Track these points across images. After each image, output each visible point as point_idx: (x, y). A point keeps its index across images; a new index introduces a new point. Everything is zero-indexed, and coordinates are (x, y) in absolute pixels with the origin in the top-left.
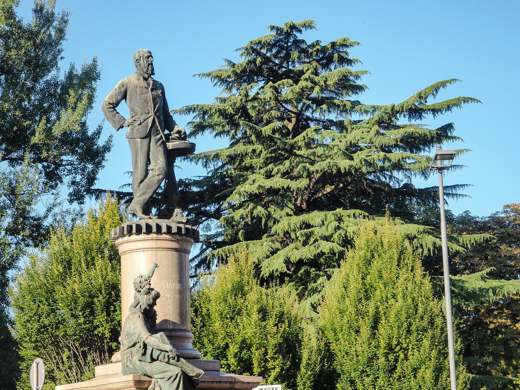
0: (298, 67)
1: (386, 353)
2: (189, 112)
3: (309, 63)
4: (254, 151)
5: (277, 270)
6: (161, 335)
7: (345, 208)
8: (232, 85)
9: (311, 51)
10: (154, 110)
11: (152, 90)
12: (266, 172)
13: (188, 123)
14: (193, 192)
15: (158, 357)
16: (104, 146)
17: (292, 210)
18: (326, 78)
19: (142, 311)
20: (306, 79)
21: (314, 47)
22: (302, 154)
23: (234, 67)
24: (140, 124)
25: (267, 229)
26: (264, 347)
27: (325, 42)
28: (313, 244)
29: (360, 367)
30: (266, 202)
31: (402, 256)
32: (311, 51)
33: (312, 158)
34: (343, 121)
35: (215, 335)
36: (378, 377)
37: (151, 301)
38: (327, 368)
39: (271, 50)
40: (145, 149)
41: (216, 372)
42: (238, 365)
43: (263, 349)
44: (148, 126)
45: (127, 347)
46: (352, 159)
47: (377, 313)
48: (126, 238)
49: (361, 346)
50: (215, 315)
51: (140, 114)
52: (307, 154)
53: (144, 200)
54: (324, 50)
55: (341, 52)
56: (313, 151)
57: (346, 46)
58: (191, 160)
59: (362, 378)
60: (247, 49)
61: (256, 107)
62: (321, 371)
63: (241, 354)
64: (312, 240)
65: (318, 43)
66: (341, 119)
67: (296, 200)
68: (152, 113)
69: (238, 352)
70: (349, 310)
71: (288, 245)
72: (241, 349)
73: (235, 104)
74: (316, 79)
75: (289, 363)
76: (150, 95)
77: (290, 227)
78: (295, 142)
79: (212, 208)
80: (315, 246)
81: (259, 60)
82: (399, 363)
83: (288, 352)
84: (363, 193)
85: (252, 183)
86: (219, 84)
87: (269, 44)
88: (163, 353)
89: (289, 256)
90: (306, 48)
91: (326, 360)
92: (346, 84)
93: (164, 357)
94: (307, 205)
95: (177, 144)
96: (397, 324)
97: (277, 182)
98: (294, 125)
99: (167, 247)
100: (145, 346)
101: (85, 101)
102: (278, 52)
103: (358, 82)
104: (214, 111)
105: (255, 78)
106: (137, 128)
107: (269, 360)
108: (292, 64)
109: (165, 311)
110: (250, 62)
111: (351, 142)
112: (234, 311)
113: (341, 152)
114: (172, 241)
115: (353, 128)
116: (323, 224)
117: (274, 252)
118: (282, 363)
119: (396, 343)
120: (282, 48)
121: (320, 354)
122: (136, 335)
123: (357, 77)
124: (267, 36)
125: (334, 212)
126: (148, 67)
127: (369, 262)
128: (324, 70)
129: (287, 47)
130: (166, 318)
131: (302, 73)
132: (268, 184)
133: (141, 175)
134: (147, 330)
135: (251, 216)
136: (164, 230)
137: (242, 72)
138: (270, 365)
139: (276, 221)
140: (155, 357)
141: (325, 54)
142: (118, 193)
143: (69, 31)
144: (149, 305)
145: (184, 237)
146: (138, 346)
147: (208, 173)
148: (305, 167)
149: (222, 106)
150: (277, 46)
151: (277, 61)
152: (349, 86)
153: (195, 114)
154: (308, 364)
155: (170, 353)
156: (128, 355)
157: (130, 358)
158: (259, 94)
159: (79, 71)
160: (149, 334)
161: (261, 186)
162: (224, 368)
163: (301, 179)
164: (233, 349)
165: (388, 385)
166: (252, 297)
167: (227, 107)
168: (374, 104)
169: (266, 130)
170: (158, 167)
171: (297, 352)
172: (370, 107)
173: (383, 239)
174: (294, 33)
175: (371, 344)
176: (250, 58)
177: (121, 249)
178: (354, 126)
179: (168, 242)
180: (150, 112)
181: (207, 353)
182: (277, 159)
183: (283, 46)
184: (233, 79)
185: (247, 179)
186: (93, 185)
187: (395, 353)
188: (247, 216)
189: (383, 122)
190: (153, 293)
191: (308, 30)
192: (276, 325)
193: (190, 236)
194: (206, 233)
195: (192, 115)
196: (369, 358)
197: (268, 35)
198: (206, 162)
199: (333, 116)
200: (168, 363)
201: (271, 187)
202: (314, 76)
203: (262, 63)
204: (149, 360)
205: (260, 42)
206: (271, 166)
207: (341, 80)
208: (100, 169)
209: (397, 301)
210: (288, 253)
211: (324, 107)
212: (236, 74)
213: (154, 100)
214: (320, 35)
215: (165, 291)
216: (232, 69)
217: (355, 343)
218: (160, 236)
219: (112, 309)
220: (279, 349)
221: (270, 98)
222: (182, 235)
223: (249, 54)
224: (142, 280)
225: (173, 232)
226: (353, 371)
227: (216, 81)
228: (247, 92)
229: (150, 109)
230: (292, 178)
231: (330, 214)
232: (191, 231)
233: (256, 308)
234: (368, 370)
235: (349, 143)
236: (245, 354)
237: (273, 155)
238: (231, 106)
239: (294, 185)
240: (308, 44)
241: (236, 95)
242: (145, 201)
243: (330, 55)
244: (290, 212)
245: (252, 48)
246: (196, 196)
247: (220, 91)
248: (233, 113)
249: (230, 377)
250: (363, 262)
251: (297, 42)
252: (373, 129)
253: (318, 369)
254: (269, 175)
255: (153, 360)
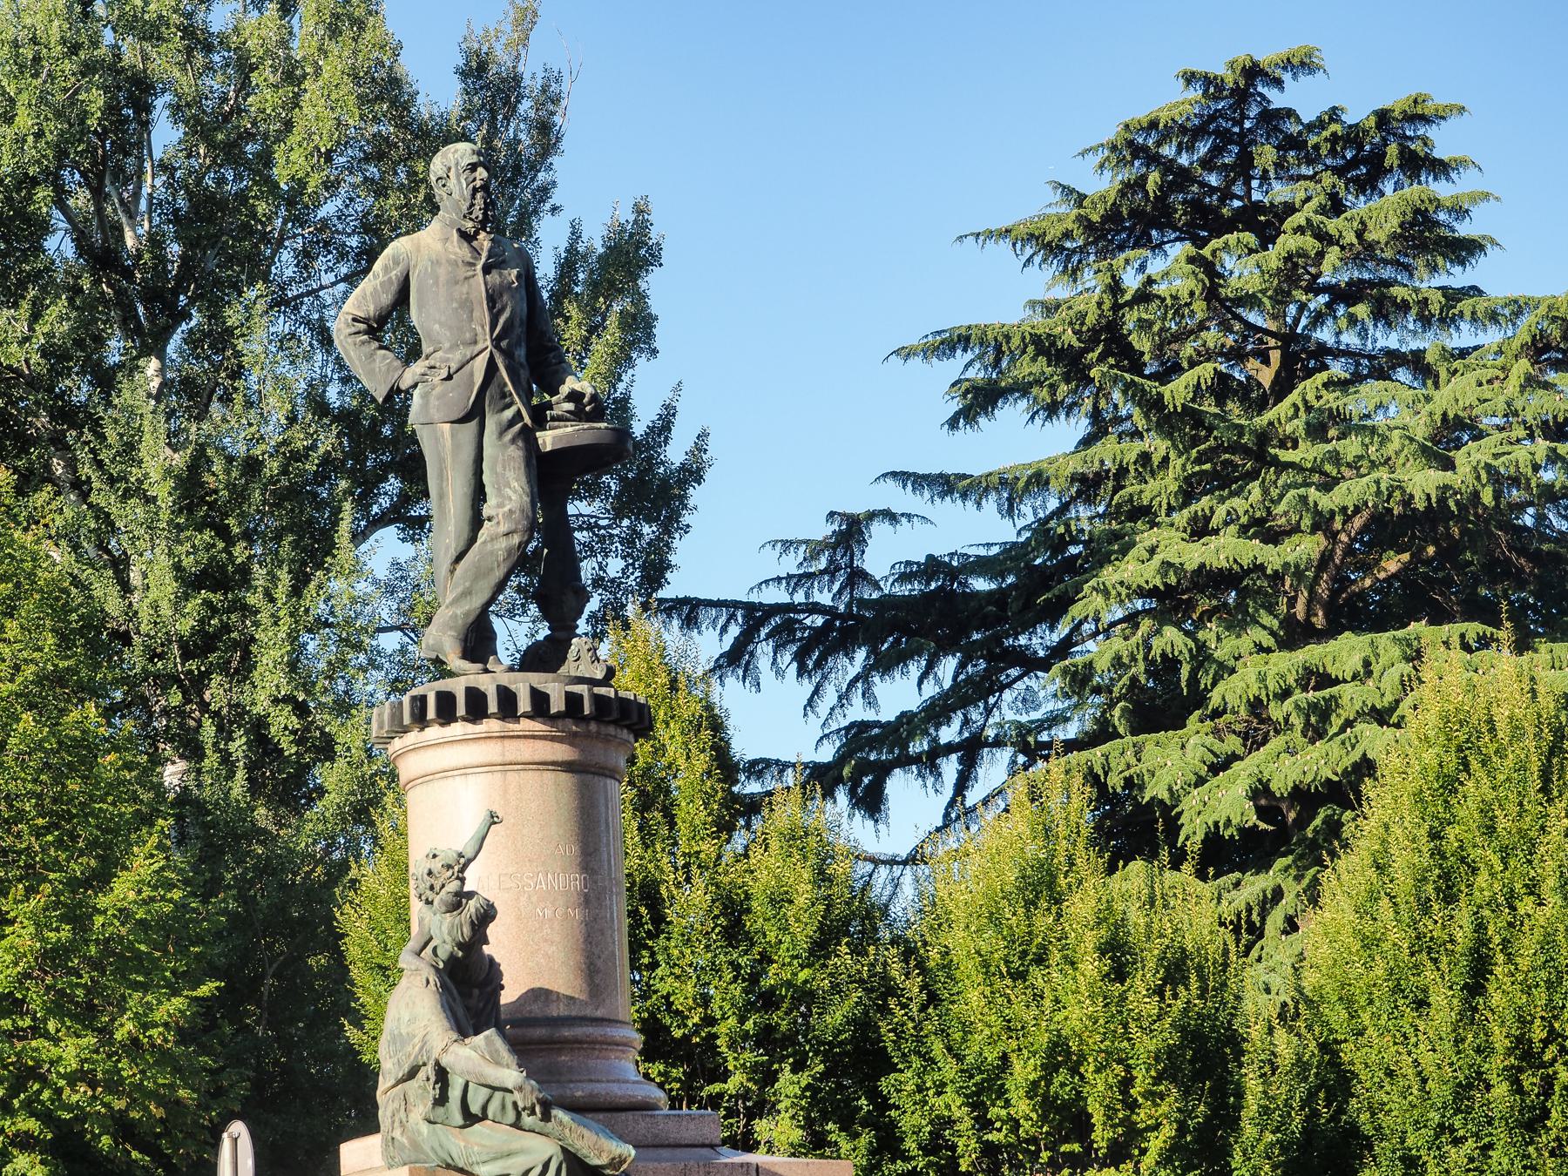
0: (1281, 192)
1: (1513, 1067)
2: (953, 349)
3: (1311, 178)
4: (1145, 458)
5: (1229, 821)
6: (487, 1038)
7: (1435, 620)
8: (1080, 261)
9: (1313, 140)
10: (492, 329)
11: (487, 270)
12: (1194, 519)
13: (953, 385)
14: (976, 595)
15: (484, 1108)
16: (683, 467)
17: (1273, 633)
18: (1362, 223)
19: (441, 965)
20: (1299, 230)
21: (1323, 129)
22: (1297, 460)
23: (1080, 206)
24: (449, 377)
25: (1198, 698)
26: (1120, 1061)
27: (1357, 113)
28: (1337, 734)
29: (1432, 1115)
30: (1203, 613)
31: (1555, 761)
32: (1313, 140)
33: (1328, 468)
34: (1425, 350)
35: (967, 1029)
36: (1490, 1146)
37: (467, 930)
38: (1328, 1121)
39: (1191, 148)
40: (468, 454)
41: (705, 1151)
42: (1044, 1118)
43: (1119, 1069)
44: (472, 384)
45: (393, 1082)
46: (1449, 465)
47: (1481, 941)
48: (413, 737)
49: (1432, 1048)
50: (968, 967)
51: (447, 345)
52: (1311, 458)
53: (466, 614)
54: (1354, 136)
55: (1411, 139)
56: (1329, 447)
57: (1425, 119)
58: (964, 496)
59: (1439, 1148)
60: (1114, 148)
61: (1150, 324)
62: (1309, 1130)
63: (1049, 1083)
64: (1336, 723)
65: (1334, 114)
66: (1415, 345)
67: (1292, 602)
68: (486, 342)
69: (1041, 1078)
70: (1393, 936)
71: (1265, 741)
72: (1050, 1068)
73: (1082, 316)
74: (1332, 225)
75: (1202, 1108)
76: (478, 286)
77: (1266, 687)
78: (1271, 423)
79: (1040, 640)
80: (1343, 743)
81: (1154, 178)
82: (1555, 1098)
83: (1198, 1076)
84: (1497, 570)
85: (1146, 555)
86: (1037, 259)
87: (1183, 129)
88: (498, 1095)
89: (1266, 776)
90: (1300, 133)
91: (1322, 1095)
92: (1428, 237)
93: (503, 1107)
94: (1326, 616)
95: (567, 435)
96: (1544, 974)
97: (1226, 549)
98: (1278, 374)
99: (537, 758)
100: (442, 1075)
101: (612, 331)
102: (1216, 151)
103: (1464, 230)
104: (1016, 341)
105: (1154, 233)
106: (438, 390)
107: (1141, 1100)
108: (1261, 186)
109: (529, 959)
110: (1128, 188)
111: (1445, 414)
112: (1024, 954)
113: (1414, 446)
114: (553, 739)
115: (1456, 371)
116: (1369, 673)
117: (1219, 766)
118: (1179, 1110)
119: (1544, 1035)
120: (1225, 138)
121: (1305, 1079)
122: (416, 1040)
123: (1460, 212)
124: (1176, 105)
125: (1400, 633)
126: (473, 197)
127: (1449, 785)
128: (1362, 198)
129: (1242, 134)
130: (537, 985)
131: (1290, 209)
132: (1194, 555)
133: (458, 538)
134: (447, 1025)
135: (1145, 658)
136: (524, 705)
137: (1105, 218)
138: (1142, 1117)
139: (1225, 670)
140: (475, 1108)
141: (1360, 148)
142: (750, 608)
143: (568, 122)
144: (460, 946)
145: (593, 727)
146: (421, 1075)
147: (1019, 533)
148: (1304, 499)
149: (1041, 324)
150: (1210, 134)
151: (1213, 180)
152: (1435, 243)
153: (969, 356)
154: (1265, 1111)
155: (517, 1096)
156: (396, 1105)
157: (402, 1114)
158: (1154, 282)
159: (595, 239)
160: (455, 1036)
161: (1170, 565)
162: (999, 1130)
163: (1295, 538)
164: (1024, 1071)
165: (1525, 1167)
166: (1081, 907)
167: (1060, 329)
168: (1515, 295)
169: (1177, 391)
170: (506, 509)
171: (1231, 1073)
172: (1501, 303)
173: (1494, 710)
174: (1260, 89)
175: (1463, 1040)
176: (1126, 174)
177: (408, 768)
178: (1457, 364)
179: (540, 744)
180: (480, 337)
181: (944, 1085)
182: (1224, 480)
183: (1228, 130)
184: (1081, 243)
185: (1134, 544)
186: (660, 586)
187: (1543, 1065)
188: (1133, 659)
189: (1548, 348)
190: (472, 906)
191: (1302, 78)
192: (1159, 992)
193: (615, 723)
194: (1018, 718)
195: (961, 358)
196: (1460, 1085)
197: (1179, 101)
198: (1010, 500)
199: (1387, 339)
200: (517, 1125)
201: (1202, 565)
202: (1324, 218)
203: (1165, 189)
204: (458, 1119)
205: (1153, 125)
206: (1206, 501)
207: (1412, 224)
208: (677, 536)
209: (1540, 904)
210: (1262, 767)
211: (1361, 310)
212: (1087, 225)
213: (492, 299)
214: (1343, 90)
215: (534, 899)
216: (1075, 211)
217: (1413, 1040)
218: (511, 726)
219: (646, 961)
220: (1170, 1067)
221: (1192, 294)
222: (586, 719)
223: (1121, 161)
224: (436, 865)
225: (553, 710)
226: (1410, 1129)
227: (1029, 251)
228: (1113, 277)
229: (479, 329)
230: (1273, 537)
231: (1384, 639)
232: (615, 706)
233: (1091, 940)
234: (1457, 1125)
235: (1438, 418)
236: (1063, 1085)
237: (1207, 466)
238: (1071, 323)
239: (1273, 557)
240: (1305, 121)
241: (1086, 292)
242: (471, 619)
243: (1382, 149)
244: (1268, 641)
245: (1130, 143)
246: (989, 603)
247: (1043, 281)
248: (1076, 344)
249: (742, 1165)
250: (1436, 785)
251: (1272, 118)
252: (1514, 370)
253: (1296, 1124)
254: (1200, 529)
255: (470, 1119)
